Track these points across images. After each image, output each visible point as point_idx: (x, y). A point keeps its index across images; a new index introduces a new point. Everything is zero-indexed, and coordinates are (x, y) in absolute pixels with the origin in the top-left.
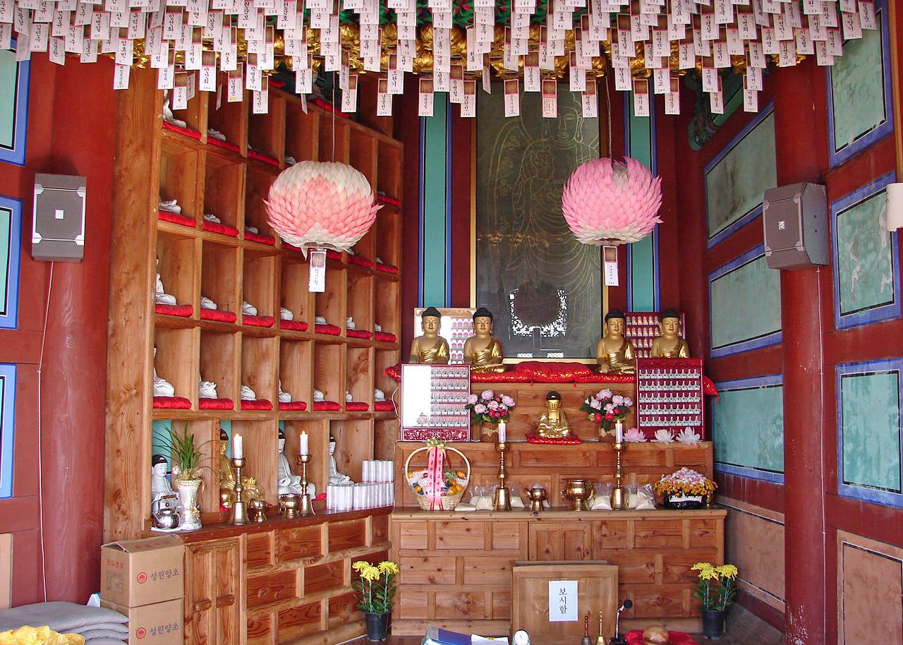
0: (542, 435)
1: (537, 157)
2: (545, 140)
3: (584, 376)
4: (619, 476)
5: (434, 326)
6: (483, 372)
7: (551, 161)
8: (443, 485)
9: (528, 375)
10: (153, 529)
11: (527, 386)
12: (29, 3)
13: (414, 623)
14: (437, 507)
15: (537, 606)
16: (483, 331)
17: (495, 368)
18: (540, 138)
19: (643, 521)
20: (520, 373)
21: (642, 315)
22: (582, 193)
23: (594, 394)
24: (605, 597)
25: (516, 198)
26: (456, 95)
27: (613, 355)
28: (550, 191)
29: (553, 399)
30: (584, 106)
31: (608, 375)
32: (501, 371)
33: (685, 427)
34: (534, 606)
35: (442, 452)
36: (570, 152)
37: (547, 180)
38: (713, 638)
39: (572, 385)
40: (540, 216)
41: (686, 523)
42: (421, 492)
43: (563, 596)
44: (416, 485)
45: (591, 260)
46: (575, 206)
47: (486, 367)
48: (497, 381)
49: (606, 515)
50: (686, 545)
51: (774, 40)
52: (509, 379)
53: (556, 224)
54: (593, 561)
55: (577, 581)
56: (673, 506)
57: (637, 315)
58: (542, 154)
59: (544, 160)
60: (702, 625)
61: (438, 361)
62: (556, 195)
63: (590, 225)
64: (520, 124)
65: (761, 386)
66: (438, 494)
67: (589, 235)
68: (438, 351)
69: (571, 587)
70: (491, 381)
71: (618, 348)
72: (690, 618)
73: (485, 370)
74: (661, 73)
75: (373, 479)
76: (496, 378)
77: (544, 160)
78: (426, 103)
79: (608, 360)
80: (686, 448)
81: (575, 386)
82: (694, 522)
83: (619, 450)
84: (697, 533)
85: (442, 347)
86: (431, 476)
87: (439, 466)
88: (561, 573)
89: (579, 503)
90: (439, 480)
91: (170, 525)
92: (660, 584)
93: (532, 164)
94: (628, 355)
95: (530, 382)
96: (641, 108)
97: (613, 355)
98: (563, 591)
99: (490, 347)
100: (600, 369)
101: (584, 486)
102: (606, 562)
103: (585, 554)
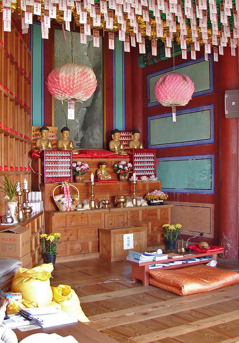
0: (102, 179)
4: (135, 194)
8: (71, 200)
10: (2, 224)
12: (120, 1)
13: (63, 257)
14: (69, 210)
15: (119, 244)
16: (45, 136)
19: (144, 212)
23: (118, 162)
24: (143, 239)
29: (104, 165)
30: (94, 42)
33: (151, 175)
34: (118, 245)
35: (68, 187)
38: (173, 250)
39: (107, 159)
41: (159, 210)
42: (63, 203)
43: (128, 240)
44: (59, 201)
45: (61, 107)
49: (132, 209)
50: (159, 218)
51: (50, 2)
54: (128, 227)
55: (133, 234)
56: (154, 204)
60: (165, 247)
65: (194, 159)
66: (70, 204)
69: (131, 236)
72: (160, 245)
74: (207, 46)
75: (34, 199)
80: (153, 182)
82: (161, 209)
83: (135, 184)
84: (162, 214)
86: (66, 197)
87: (69, 192)
88: (128, 231)
89: (122, 205)
90: (70, 198)
91: (11, 222)
92: (150, 233)
94: (122, 147)
96: (184, 56)
98: (128, 238)
101: (125, 198)
102: (133, 226)
103: (125, 224)
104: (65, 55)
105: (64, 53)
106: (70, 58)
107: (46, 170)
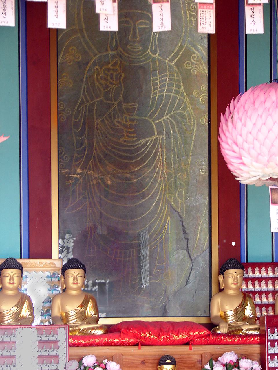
1: (102, 74)
2: (113, 53)
3: (201, 337)
5: (16, 280)
6: (78, 334)
7: (120, 78)
9: (135, 336)
11: (133, 350)
16: (11, 286)
17: (93, 329)
18: (107, 50)
20: (126, 334)
21: (260, 265)
22: (249, 124)
25: (76, 125)
26: (103, 4)
27: (230, 313)
28: (118, 117)
31: (228, 335)
32: (100, 332)
36: (141, 67)
37: (116, 104)
40: (106, 147)
45: (168, 202)
46: (240, 140)
47: (82, 327)
48: (98, 345)
52: (113, 342)
53: (125, 158)
57: (254, 265)
58: (108, 70)
59: (112, 78)
61: (23, 322)
62: (126, 121)
63: (257, 162)
64: (81, 30)
67: (253, 174)
68: (21, 311)
70: (90, 345)
71: (236, 304)
73: (81, 332)
76: (97, 341)
77: (112, 78)
78: (57, 11)
79: (225, 318)
81: (191, 349)
85: (26, 305)
93: (96, 83)
94: (248, 312)
95: (137, 345)
97: (230, 313)
99: (84, 305)
100: (219, 329)
104: (179, 51)
105: (176, 46)
106: (194, 57)
107: (268, 336)
